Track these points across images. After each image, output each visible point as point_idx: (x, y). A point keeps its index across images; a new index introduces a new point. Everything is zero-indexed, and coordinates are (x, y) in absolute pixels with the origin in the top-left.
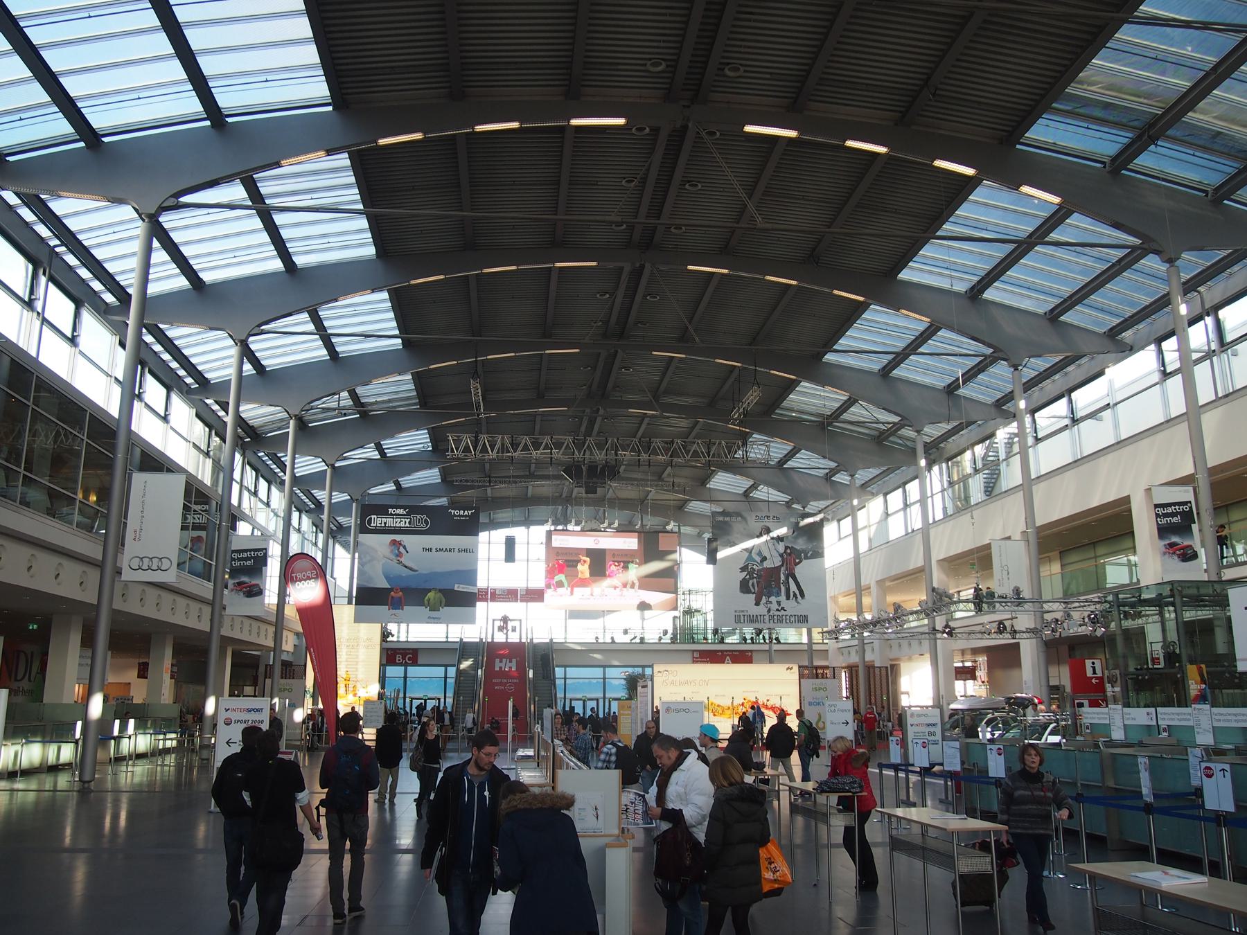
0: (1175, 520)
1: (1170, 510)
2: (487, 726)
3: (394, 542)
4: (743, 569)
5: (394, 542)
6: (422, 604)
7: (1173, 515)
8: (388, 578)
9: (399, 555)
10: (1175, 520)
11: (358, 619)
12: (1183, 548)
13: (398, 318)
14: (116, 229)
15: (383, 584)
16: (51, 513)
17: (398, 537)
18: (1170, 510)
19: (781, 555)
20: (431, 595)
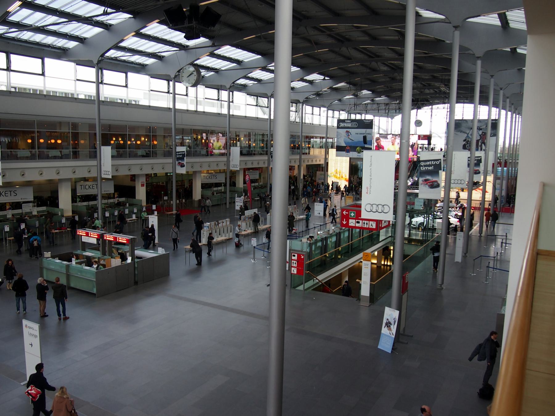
0: (430, 168)
1: (428, 163)
2: (303, 200)
3: (347, 131)
4: (464, 141)
5: (347, 131)
6: (355, 151)
7: (429, 166)
8: (345, 143)
9: (349, 135)
10: (430, 168)
11: (337, 155)
12: (433, 182)
13: (527, 26)
14: (72, 4)
15: (344, 145)
16: (413, 101)
17: (348, 130)
18: (428, 163)
19: (480, 135)
20: (358, 148)
